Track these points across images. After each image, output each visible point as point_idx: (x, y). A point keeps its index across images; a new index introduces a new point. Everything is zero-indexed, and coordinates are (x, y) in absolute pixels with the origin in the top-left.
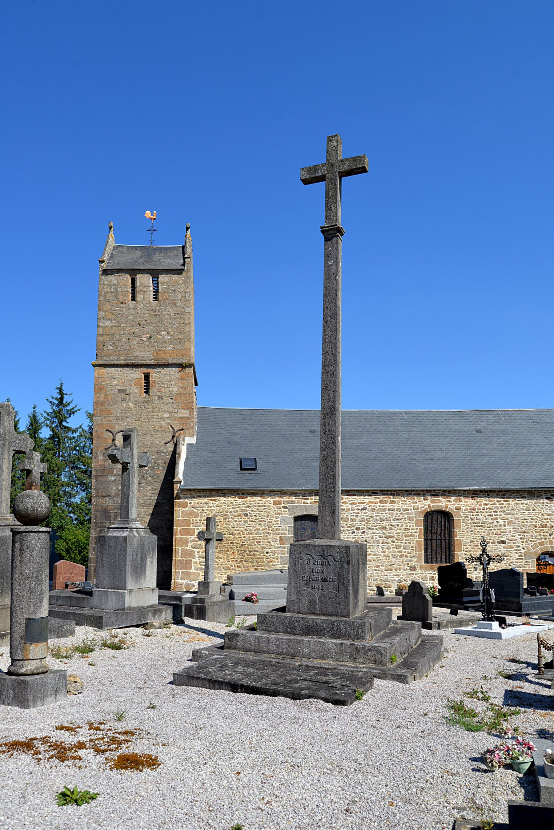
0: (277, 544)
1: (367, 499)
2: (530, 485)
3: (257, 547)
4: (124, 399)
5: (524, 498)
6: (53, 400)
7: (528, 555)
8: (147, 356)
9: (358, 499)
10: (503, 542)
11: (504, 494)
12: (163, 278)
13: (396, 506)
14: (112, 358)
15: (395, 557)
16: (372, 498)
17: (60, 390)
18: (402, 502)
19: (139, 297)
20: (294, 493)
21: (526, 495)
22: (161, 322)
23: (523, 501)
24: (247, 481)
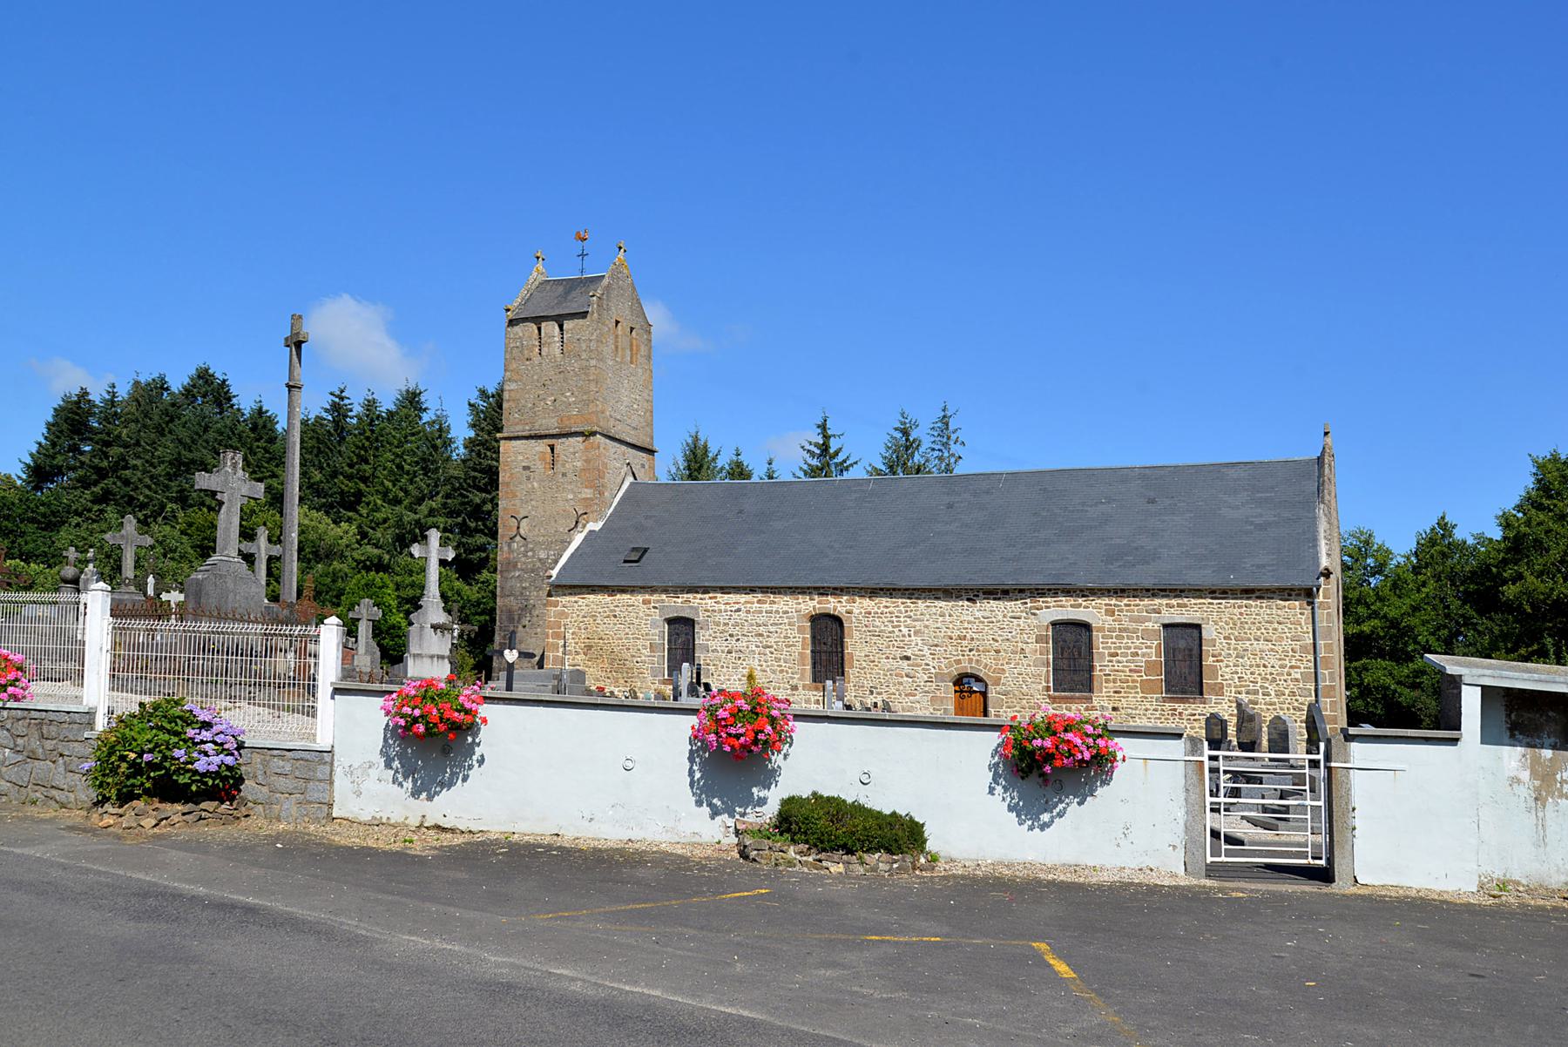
0: (646, 652)
1: (743, 598)
2: (948, 582)
3: (627, 655)
4: (528, 478)
5: (937, 599)
6: (812, 448)
7: (940, 677)
8: (550, 424)
9: (733, 597)
10: (908, 658)
11: (912, 593)
12: (567, 325)
13: (775, 607)
14: (519, 428)
15: (774, 672)
16: (749, 597)
17: (823, 427)
18: (785, 603)
19: (545, 350)
20: (665, 590)
21: (940, 594)
22: (566, 380)
23: (936, 603)
24: (633, 575)
